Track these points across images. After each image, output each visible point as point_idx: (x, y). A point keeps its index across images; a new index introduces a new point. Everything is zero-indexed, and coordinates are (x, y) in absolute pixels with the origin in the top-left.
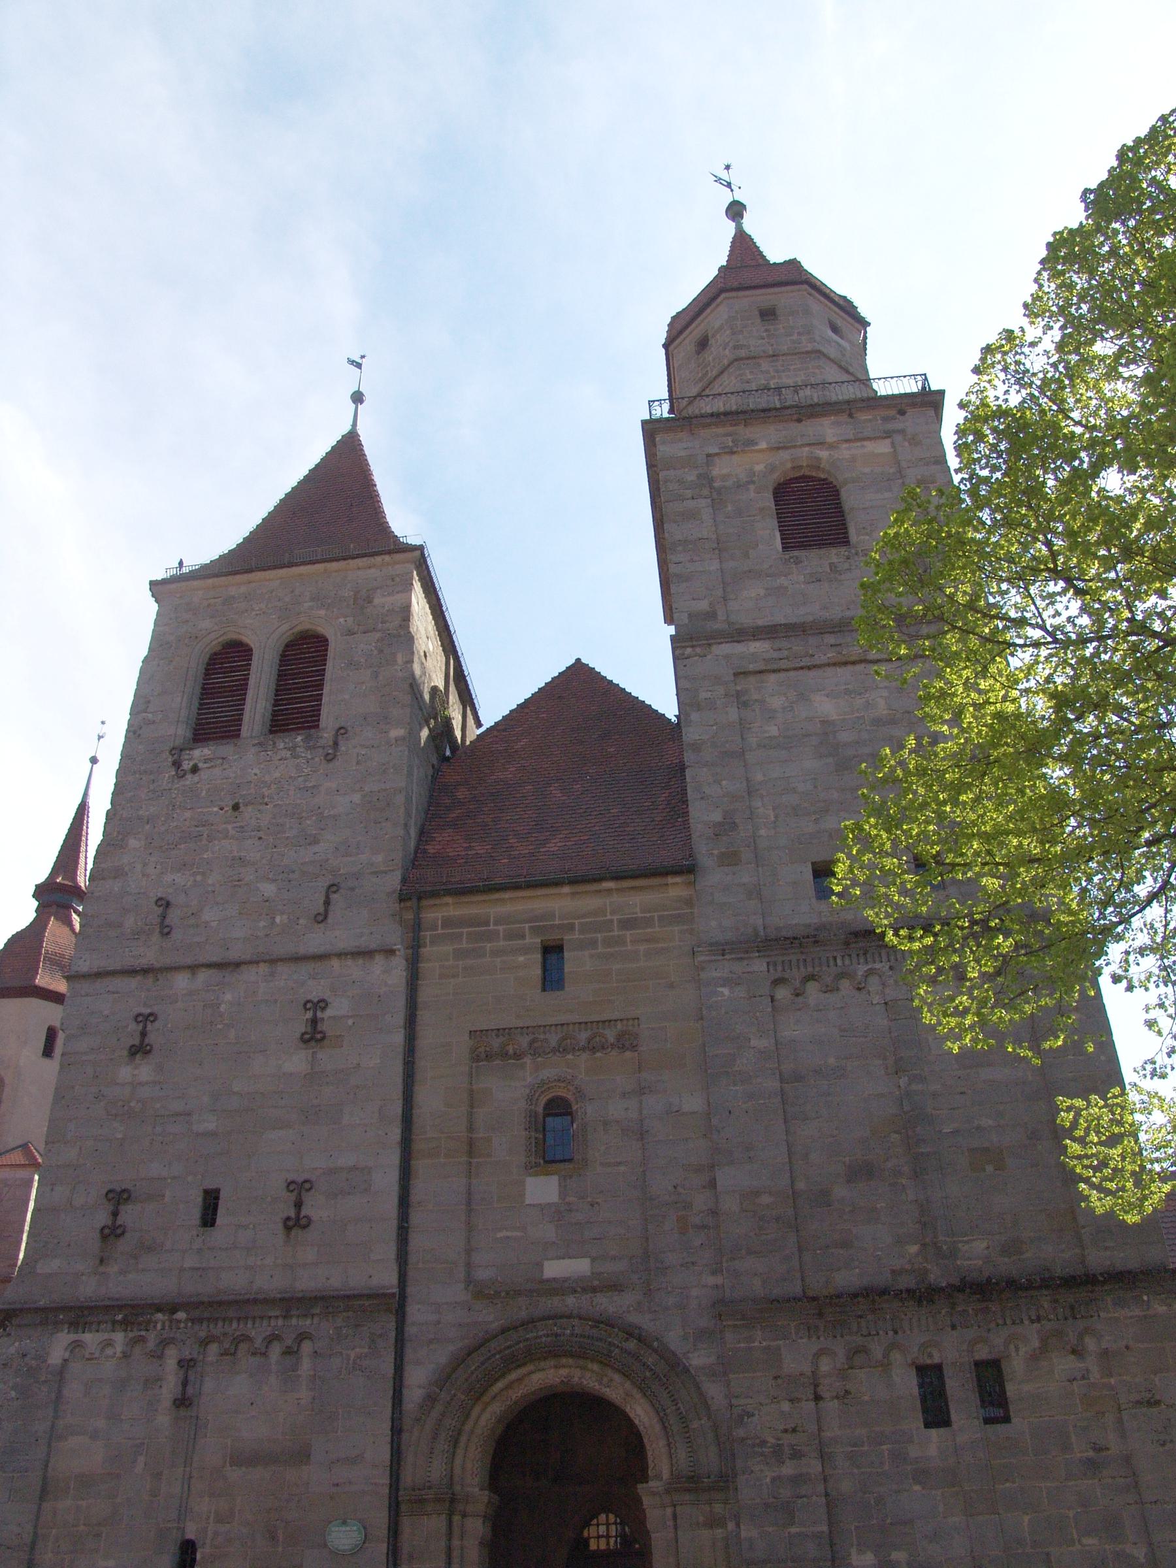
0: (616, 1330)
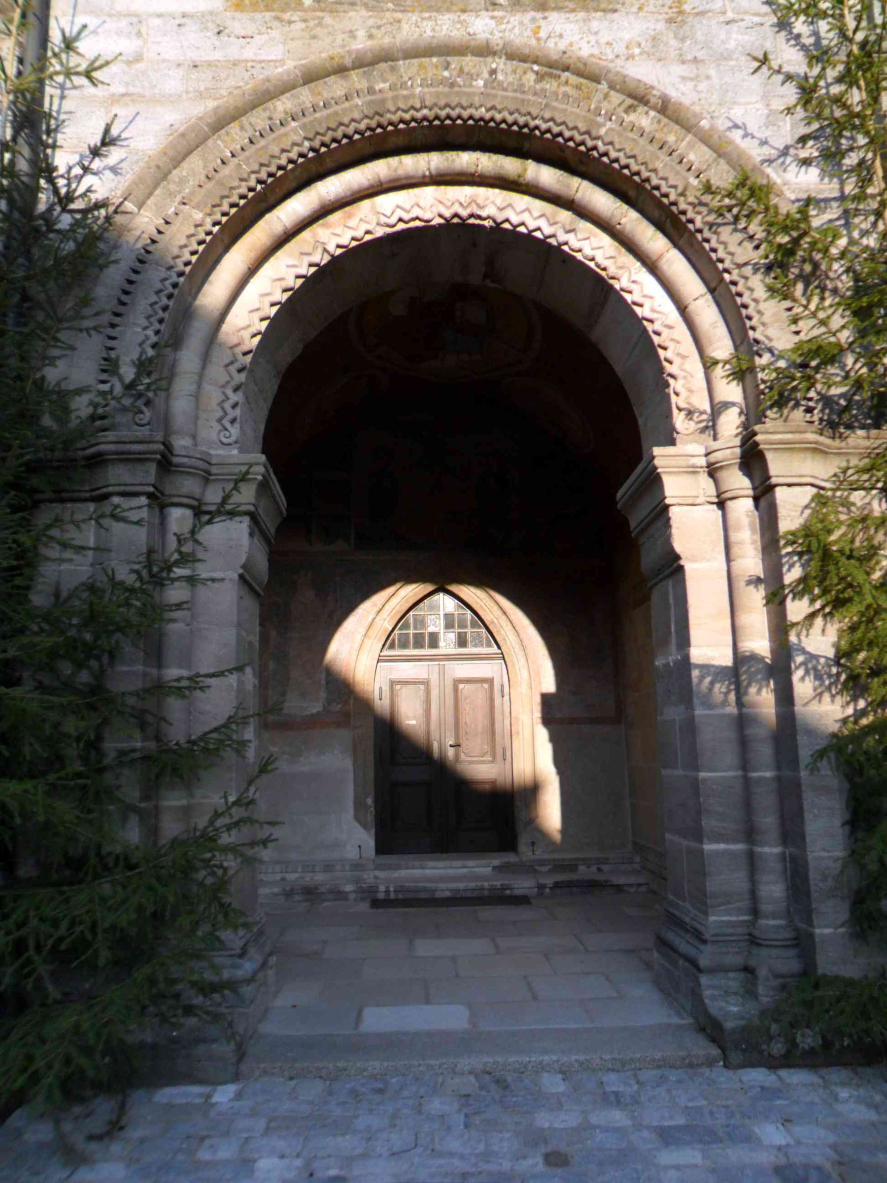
0: (604, 86)
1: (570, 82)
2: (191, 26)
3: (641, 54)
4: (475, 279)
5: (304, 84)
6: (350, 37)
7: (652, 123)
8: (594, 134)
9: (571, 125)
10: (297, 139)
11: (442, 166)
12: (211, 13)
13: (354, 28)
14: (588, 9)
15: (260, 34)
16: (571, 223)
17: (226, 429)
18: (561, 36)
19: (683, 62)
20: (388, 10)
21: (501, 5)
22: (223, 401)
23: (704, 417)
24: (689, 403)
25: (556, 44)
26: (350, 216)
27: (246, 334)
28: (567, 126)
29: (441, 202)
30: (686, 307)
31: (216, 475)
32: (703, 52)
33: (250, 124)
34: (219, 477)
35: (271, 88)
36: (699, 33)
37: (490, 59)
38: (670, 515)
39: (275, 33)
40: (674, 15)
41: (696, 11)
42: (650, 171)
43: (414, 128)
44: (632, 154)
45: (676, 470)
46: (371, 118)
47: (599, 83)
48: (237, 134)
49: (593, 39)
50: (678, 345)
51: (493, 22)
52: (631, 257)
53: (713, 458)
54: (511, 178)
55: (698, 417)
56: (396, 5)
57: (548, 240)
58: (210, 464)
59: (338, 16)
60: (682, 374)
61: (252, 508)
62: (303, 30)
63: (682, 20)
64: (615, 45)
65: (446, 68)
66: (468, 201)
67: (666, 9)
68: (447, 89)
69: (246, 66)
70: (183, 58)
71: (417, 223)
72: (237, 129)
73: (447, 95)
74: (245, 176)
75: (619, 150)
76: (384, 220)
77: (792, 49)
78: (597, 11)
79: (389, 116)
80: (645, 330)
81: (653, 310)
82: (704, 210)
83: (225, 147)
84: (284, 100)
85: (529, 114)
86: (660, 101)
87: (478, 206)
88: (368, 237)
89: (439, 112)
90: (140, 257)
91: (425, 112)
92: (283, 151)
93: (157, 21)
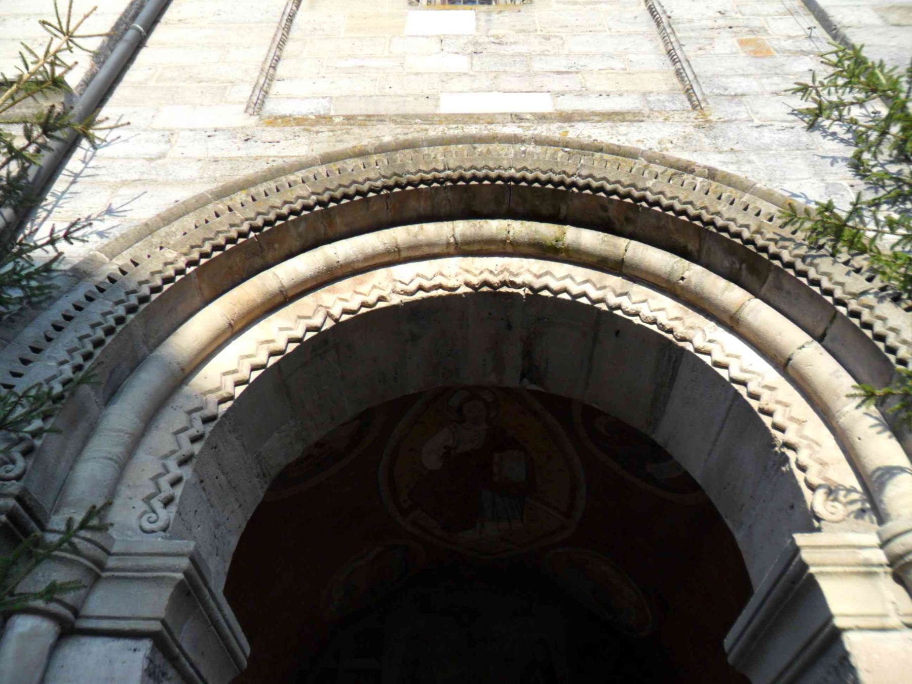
0: (642, 162)
4: (512, 379)
5: (322, 164)
11: (468, 233)
16: (622, 287)
17: (154, 512)
19: (721, 152)
22: (160, 475)
23: (855, 496)
24: (826, 479)
26: (361, 283)
27: (213, 398)
29: (467, 271)
30: (789, 359)
31: (112, 570)
34: (116, 574)
38: (848, 647)
43: (436, 188)
45: (840, 569)
50: (788, 409)
52: (701, 318)
53: (897, 547)
54: (548, 243)
55: (845, 496)
57: (597, 305)
58: (109, 554)
60: (805, 442)
61: (156, 626)
63: (711, 126)
64: (646, 141)
71: (440, 292)
76: (400, 287)
77: (831, 142)
80: (737, 394)
81: (743, 371)
82: (791, 245)
87: (511, 273)
88: (381, 305)
90: (89, 295)
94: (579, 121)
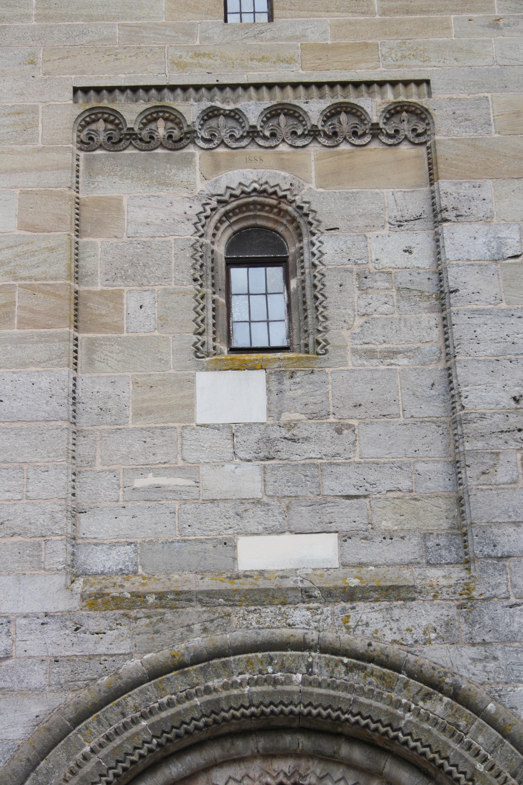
1: (375, 673)
2: (52, 628)
3: (436, 638)
6: (188, 631)
7: (446, 709)
8: (395, 725)
9: (375, 719)
10: (147, 737)
12: (69, 611)
13: (190, 623)
14: (390, 598)
15: (111, 630)
18: (367, 625)
19: (473, 645)
20: (219, 605)
21: (316, 597)
25: (363, 632)
28: (372, 720)
32: (491, 635)
33: (106, 718)
35: (122, 685)
36: (486, 618)
37: (306, 653)
39: (124, 629)
40: (465, 601)
41: (482, 597)
42: (443, 759)
44: (427, 744)
46: (208, 717)
47: (400, 673)
48: (94, 728)
49: (394, 625)
51: (308, 613)
56: (226, 600)
59: (177, 612)
62: (147, 625)
63: (472, 606)
64: (414, 631)
65: (270, 664)
66: (292, 770)
67: (457, 596)
68: (271, 688)
69: (100, 660)
70: (46, 654)
72: (95, 724)
73: (272, 693)
74: (105, 772)
75: (416, 741)
78: (397, 600)
79: (223, 714)
83: (85, 740)
84: (134, 696)
85: (340, 709)
86: (452, 688)
87: (301, 775)
89: (264, 709)
91: (253, 709)
92: (135, 748)
93: (23, 621)
94: (360, 599)
